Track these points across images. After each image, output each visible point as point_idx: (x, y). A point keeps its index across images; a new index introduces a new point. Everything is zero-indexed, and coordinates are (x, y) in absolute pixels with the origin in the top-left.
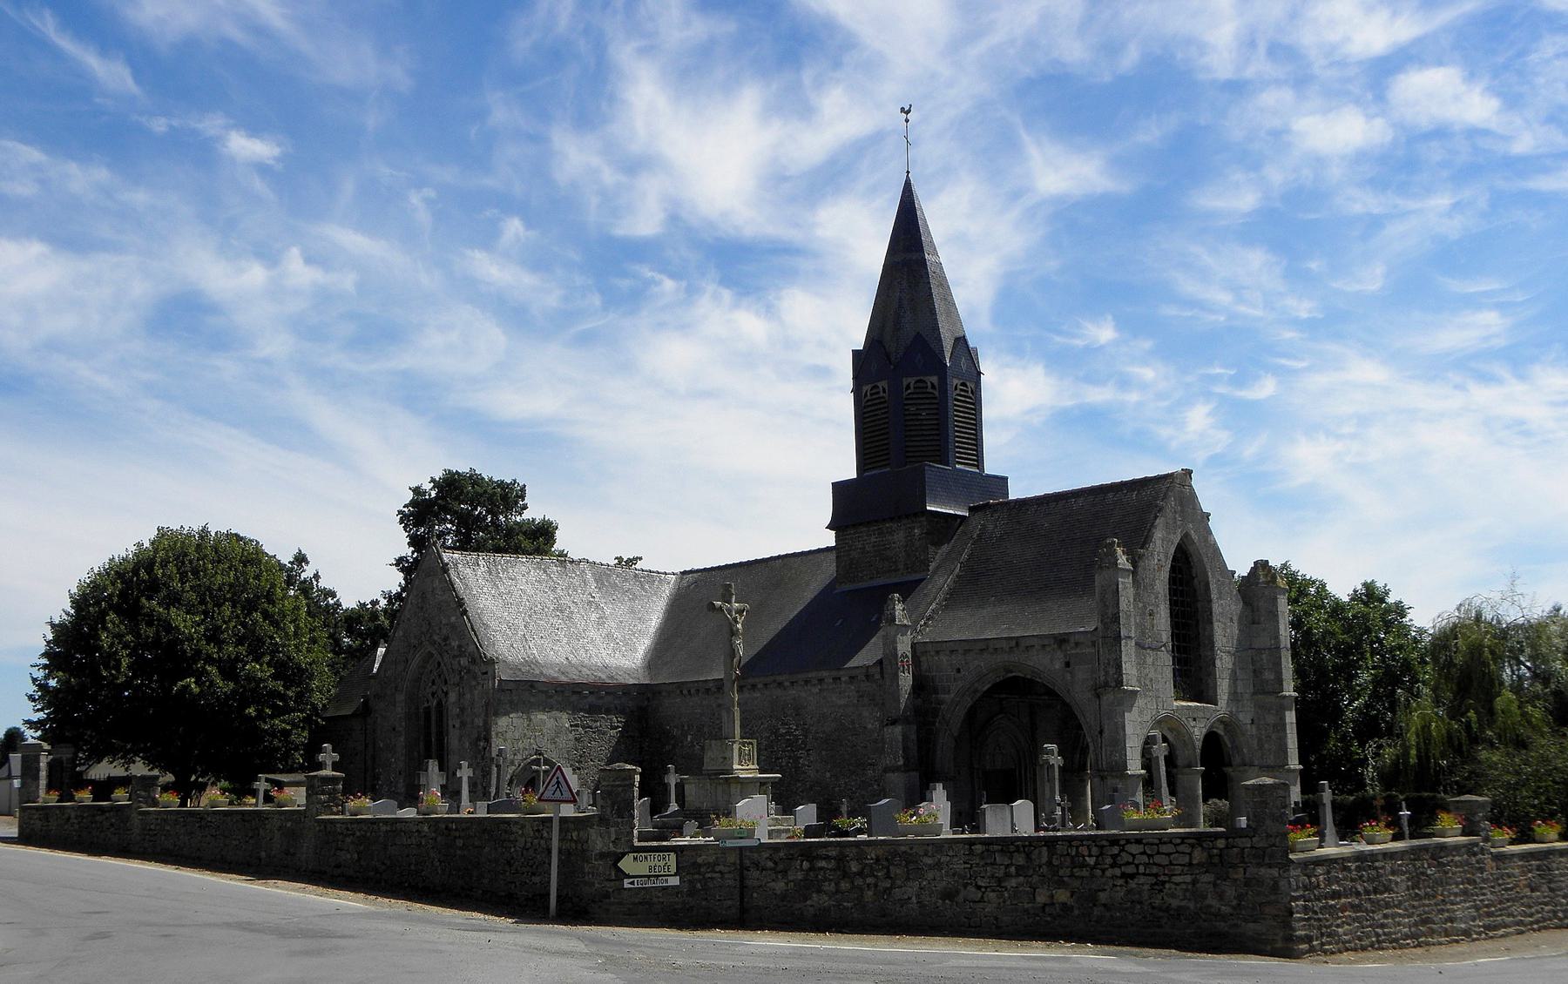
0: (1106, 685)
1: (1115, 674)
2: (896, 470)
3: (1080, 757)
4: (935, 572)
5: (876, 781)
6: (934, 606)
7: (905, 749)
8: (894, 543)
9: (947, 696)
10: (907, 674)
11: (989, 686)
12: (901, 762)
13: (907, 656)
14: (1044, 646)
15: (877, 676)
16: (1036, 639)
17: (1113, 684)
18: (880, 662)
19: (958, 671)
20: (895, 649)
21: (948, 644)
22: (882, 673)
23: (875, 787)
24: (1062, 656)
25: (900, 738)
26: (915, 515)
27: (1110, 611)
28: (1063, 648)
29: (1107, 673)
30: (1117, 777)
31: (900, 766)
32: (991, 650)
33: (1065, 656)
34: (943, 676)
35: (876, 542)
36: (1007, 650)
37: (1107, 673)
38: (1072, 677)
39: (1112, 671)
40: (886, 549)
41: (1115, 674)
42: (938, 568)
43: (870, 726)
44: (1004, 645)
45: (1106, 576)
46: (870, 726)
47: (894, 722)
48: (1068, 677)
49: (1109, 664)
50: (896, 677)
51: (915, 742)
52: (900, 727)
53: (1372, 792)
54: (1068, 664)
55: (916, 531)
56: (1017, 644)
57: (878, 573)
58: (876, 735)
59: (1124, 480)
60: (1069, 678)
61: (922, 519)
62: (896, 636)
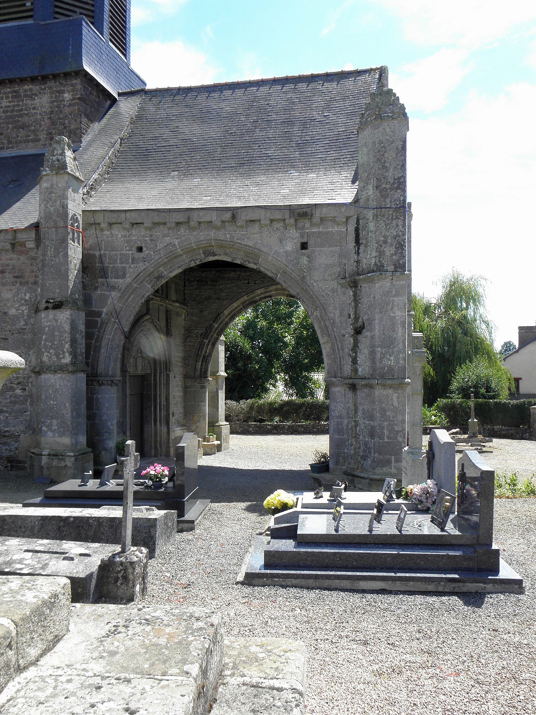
0: (379, 269)
1: (395, 254)
2: (42, 23)
3: (202, 365)
4: (90, 144)
5: (19, 383)
6: (95, 176)
7: (73, 342)
8: (34, 108)
9: (121, 281)
10: (76, 244)
11: (180, 270)
12: (67, 359)
13: (77, 220)
14: (272, 221)
15: (31, 245)
16: (263, 212)
17: (391, 268)
18: (36, 226)
19: (140, 249)
20: (65, 207)
21: (128, 214)
22: (38, 240)
23: (18, 392)
24: (298, 234)
25: (67, 327)
26: (67, 75)
27: (391, 175)
28: (300, 225)
29: (381, 253)
30: (391, 387)
31: (67, 365)
32: (192, 224)
33: (302, 236)
34: (116, 255)
35: (9, 107)
36: (219, 224)
37: (381, 253)
38: (310, 262)
39: (389, 251)
40: (21, 116)
41: (395, 254)
42: (92, 141)
43: (13, 312)
44: (213, 217)
45: (388, 130)
46: (13, 312)
47: (58, 306)
48: (304, 260)
49: (385, 242)
50: (63, 244)
51: (84, 334)
52: (68, 312)
53: (320, 395)
54: (304, 246)
55: (66, 95)
56: (234, 217)
57: (9, 142)
58: (23, 323)
59: (329, 72)
60: (305, 262)
61: (75, 82)
62: (66, 189)
